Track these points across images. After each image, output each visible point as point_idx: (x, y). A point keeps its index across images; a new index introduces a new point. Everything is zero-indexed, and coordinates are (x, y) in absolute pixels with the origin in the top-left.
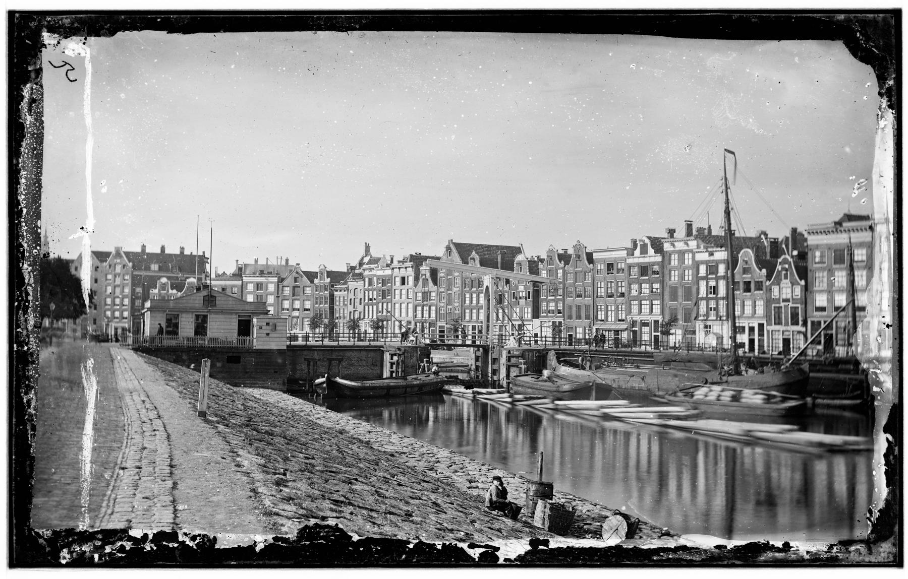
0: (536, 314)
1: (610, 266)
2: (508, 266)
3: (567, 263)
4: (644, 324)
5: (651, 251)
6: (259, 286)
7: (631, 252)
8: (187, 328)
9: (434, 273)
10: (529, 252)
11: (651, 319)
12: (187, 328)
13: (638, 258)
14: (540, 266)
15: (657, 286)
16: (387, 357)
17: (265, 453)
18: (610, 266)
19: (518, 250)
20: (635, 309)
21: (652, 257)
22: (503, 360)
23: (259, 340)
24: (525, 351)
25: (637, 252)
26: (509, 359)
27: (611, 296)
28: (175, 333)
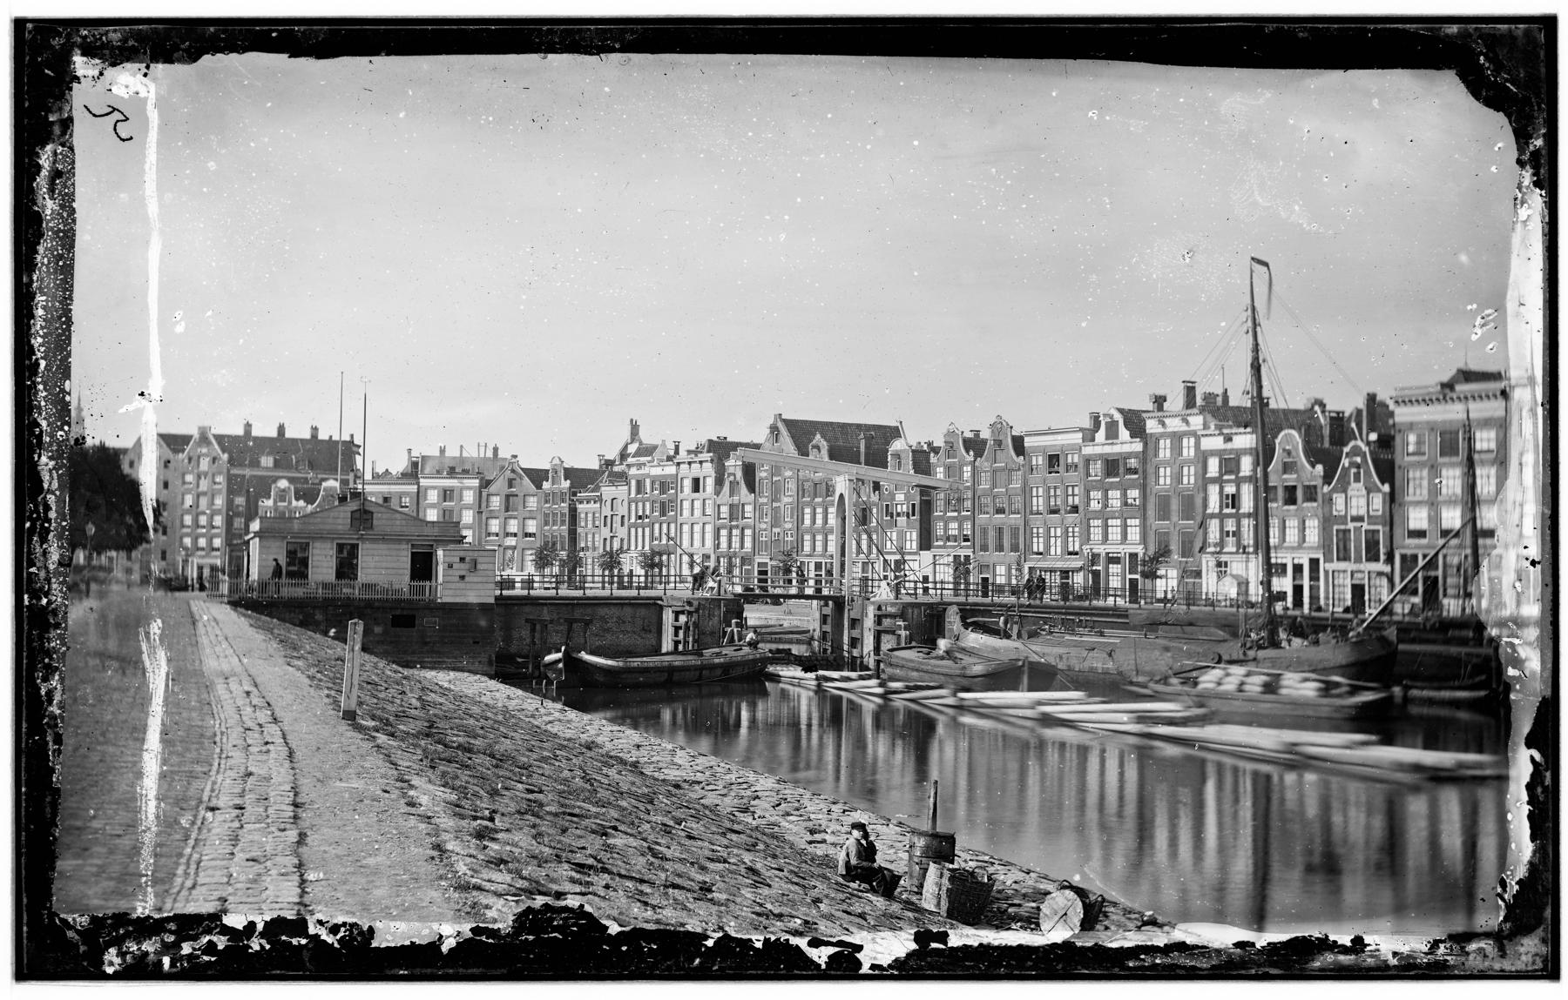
0: (925, 543)
1: (1053, 460)
2: (877, 459)
3: (979, 454)
4: (1113, 560)
5: (1124, 434)
6: (446, 494)
7: (1089, 436)
8: (322, 566)
9: (749, 471)
10: (914, 436)
11: (1124, 550)
12: (322, 566)
13: (1101, 446)
14: (933, 459)
15: (1134, 494)
16: (668, 616)
17: (458, 783)
18: (1053, 460)
19: (895, 432)
20: (1096, 534)
21: (1127, 444)
22: (869, 622)
23: (447, 587)
24: (906, 606)
25: (1100, 436)
26: (879, 620)
27: (1055, 512)
28: (303, 575)
